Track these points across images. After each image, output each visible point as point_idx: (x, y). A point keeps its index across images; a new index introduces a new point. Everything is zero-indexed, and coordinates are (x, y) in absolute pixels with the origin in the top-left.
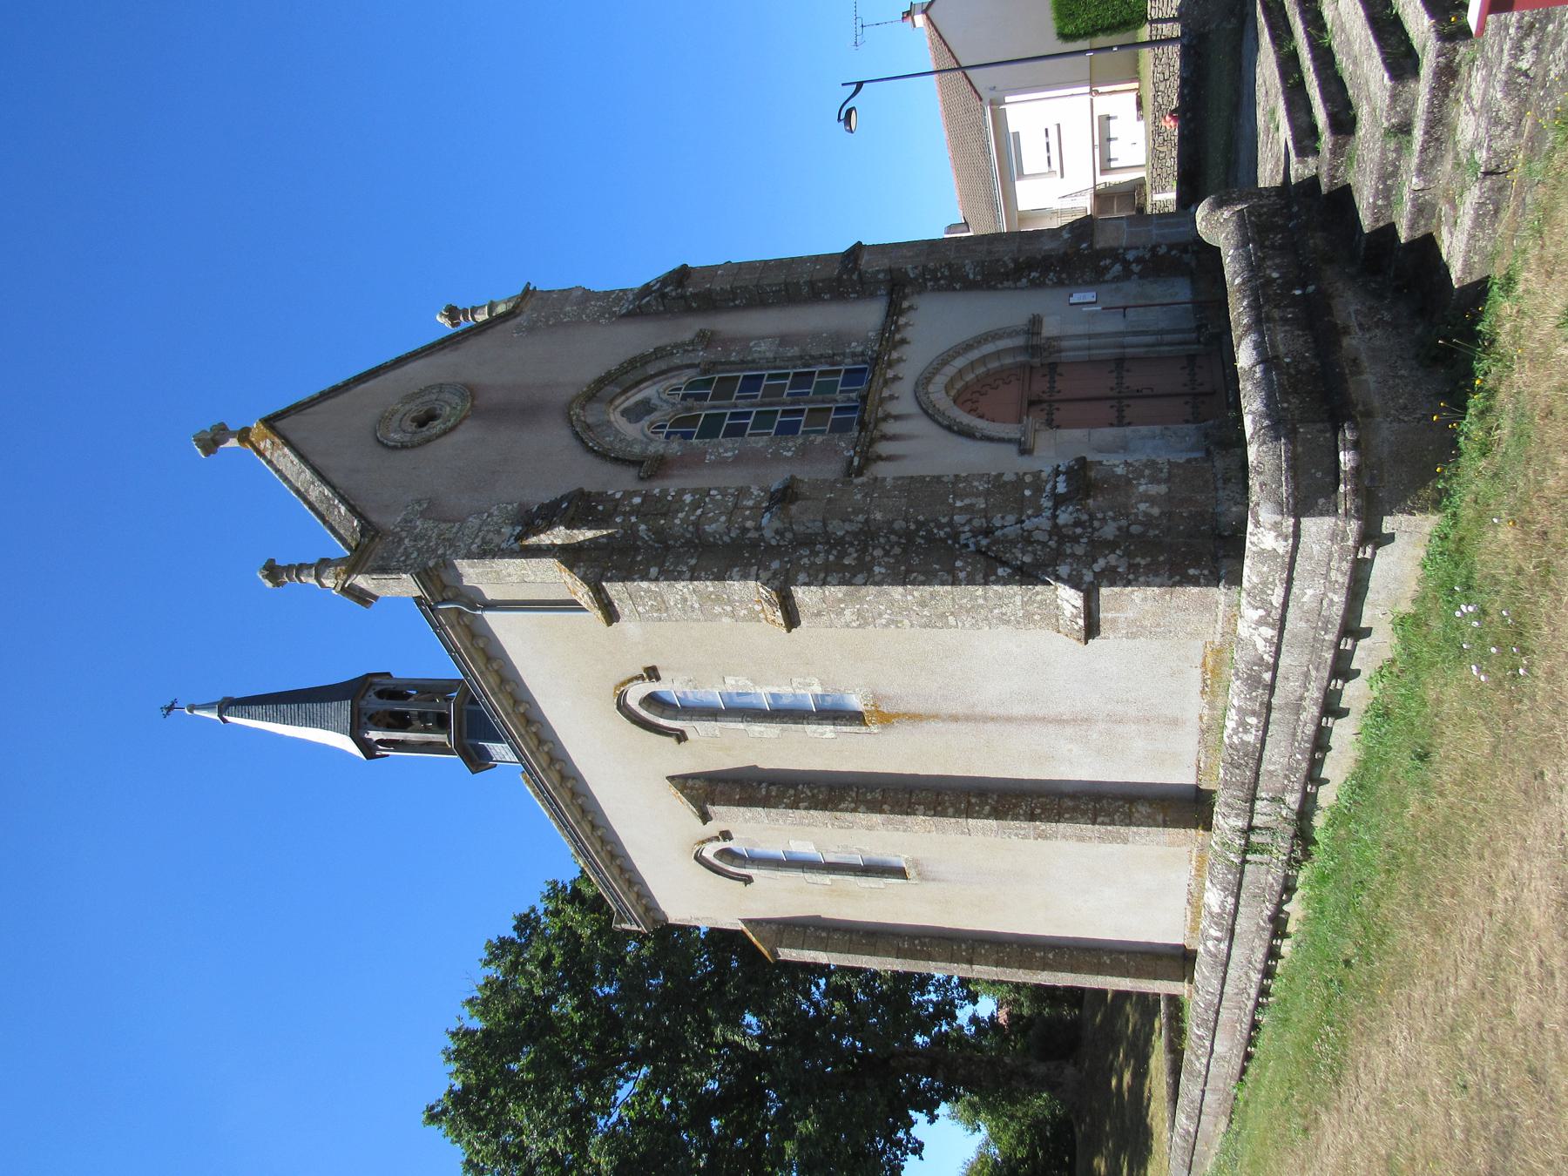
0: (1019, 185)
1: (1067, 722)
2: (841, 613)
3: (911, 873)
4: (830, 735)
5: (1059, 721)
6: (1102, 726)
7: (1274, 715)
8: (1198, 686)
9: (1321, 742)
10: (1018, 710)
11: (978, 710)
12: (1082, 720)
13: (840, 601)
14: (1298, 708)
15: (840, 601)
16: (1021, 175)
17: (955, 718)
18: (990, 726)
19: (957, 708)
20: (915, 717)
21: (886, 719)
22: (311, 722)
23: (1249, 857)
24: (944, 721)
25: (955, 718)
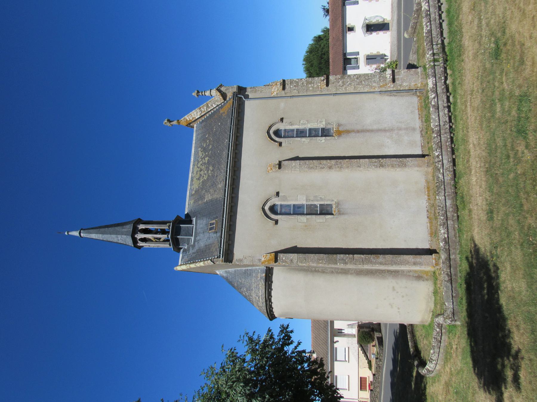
0: (335, 362)
1: (387, 130)
2: (338, 82)
3: (334, 209)
4: (323, 141)
5: (385, 130)
6: (396, 132)
7: (432, 23)
8: (418, 117)
9: (441, 24)
10: (375, 127)
11: (365, 128)
12: (391, 130)
13: (339, 79)
14: (435, 20)
15: (339, 79)
16: (336, 360)
17: (358, 132)
18: (368, 134)
19: (359, 127)
20: (348, 132)
21: (340, 133)
22: (117, 233)
23: (436, 64)
24: (355, 133)
25: (358, 132)
